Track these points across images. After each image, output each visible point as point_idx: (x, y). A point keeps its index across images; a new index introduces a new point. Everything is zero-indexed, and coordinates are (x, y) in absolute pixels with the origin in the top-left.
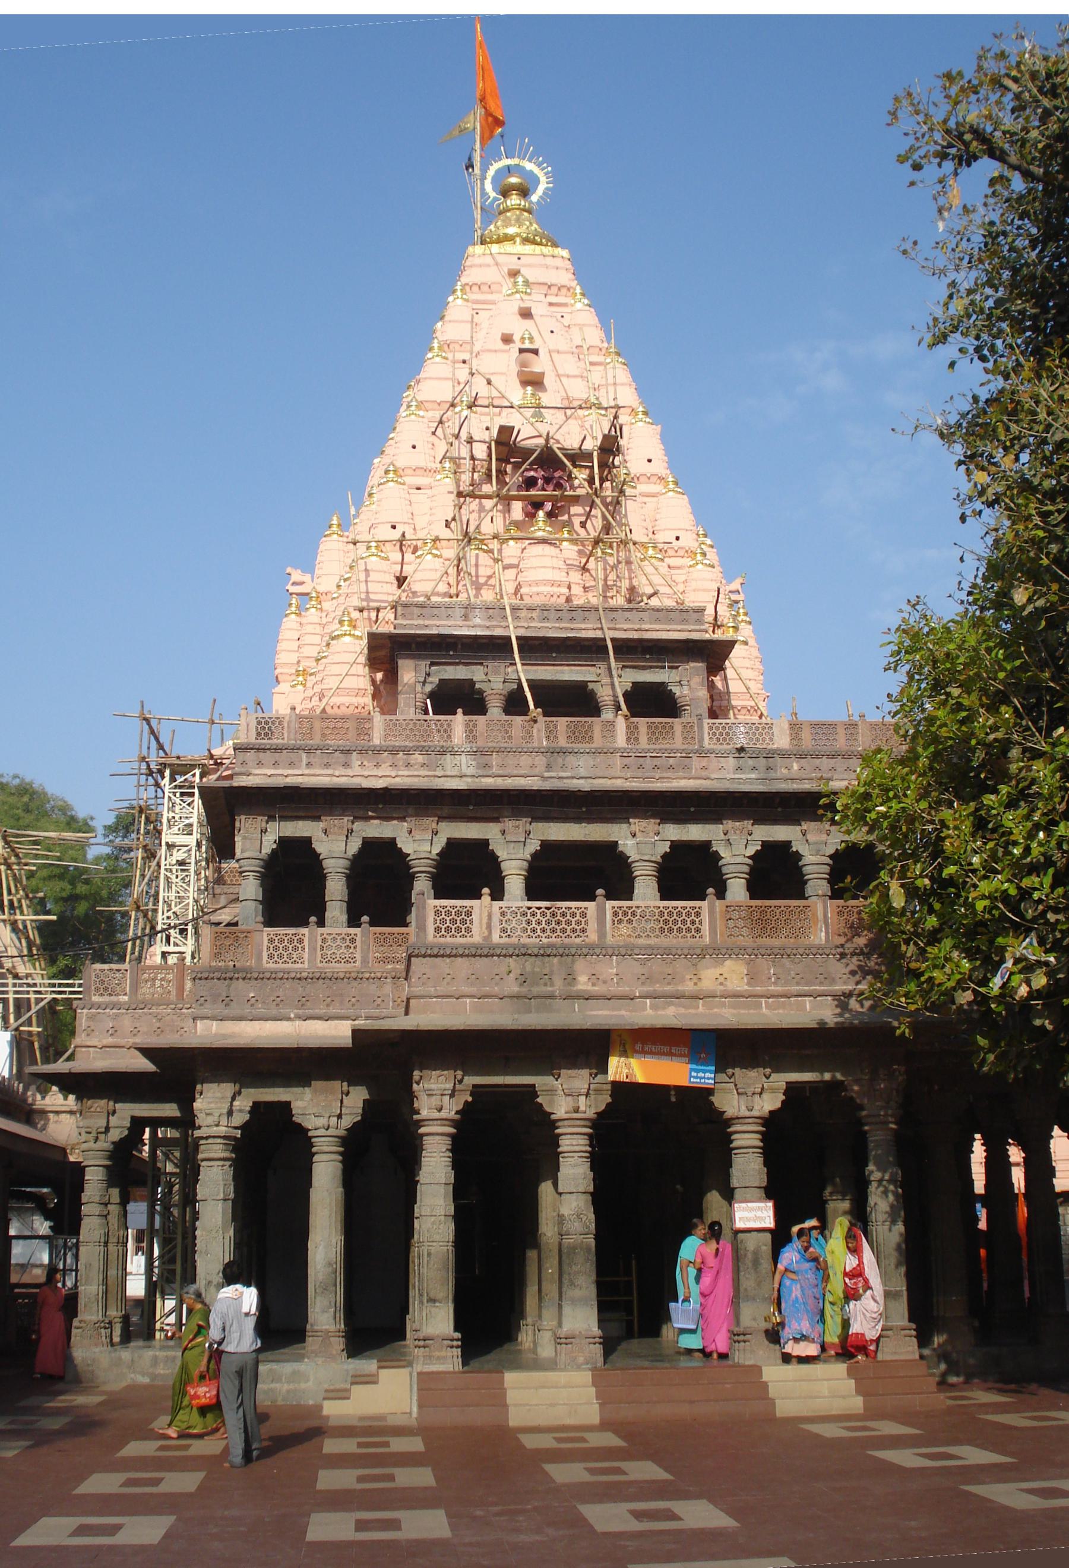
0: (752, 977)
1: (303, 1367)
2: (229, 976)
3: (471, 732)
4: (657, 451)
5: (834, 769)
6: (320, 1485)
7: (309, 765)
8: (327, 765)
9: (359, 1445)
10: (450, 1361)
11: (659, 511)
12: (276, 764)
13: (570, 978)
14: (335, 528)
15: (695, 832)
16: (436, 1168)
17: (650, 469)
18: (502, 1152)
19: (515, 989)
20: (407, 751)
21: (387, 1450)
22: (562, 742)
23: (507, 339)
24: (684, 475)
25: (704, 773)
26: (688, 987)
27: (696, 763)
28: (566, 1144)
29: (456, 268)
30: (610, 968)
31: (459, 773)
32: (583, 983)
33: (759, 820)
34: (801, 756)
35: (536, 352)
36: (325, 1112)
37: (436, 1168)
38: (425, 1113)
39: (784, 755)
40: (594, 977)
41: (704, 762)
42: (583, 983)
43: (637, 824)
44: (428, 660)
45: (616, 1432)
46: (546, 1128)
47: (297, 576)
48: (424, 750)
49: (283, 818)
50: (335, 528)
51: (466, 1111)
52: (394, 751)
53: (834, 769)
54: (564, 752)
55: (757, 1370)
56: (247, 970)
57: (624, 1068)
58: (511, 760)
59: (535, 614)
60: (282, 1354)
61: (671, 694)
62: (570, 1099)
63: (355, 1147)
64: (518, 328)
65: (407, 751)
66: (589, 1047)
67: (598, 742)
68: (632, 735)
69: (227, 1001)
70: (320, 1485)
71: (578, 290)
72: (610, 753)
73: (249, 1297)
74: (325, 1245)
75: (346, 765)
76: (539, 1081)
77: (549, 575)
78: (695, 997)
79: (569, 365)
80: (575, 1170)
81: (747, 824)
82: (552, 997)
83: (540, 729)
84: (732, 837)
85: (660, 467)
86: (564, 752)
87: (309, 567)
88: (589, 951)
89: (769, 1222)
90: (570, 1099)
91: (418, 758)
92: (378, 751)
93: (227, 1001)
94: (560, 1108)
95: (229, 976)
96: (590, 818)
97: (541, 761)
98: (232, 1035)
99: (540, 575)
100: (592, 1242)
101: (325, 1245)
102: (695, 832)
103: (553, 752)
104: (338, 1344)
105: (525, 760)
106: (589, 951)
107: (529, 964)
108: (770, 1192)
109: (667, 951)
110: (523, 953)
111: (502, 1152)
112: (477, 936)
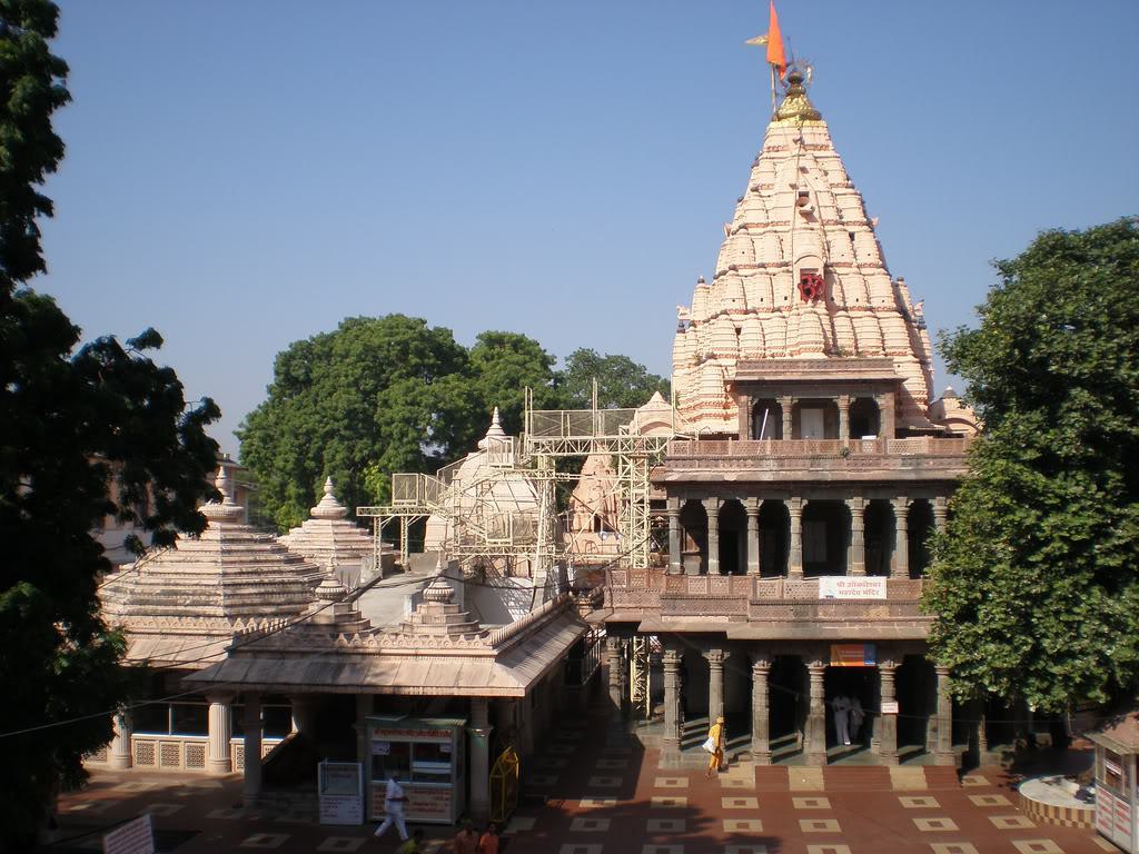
0: (891, 614)
2: (675, 598)
3: (774, 447)
5: (950, 464)
7: (699, 466)
8: (707, 466)
9: (736, 803)
10: (766, 763)
13: (816, 614)
20: (745, 459)
21: (743, 807)
22: (818, 452)
25: (886, 467)
26: (864, 617)
27: (883, 461)
28: (813, 679)
29: (764, 136)
40: (825, 614)
41: (887, 461)
42: (821, 616)
44: (766, 399)
48: (753, 458)
52: (739, 459)
53: (950, 464)
54: (818, 458)
55: (887, 769)
56: (682, 595)
58: (794, 462)
59: (806, 364)
60: (695, 752)
65: (745, 459)
69: (674, 608)
75: (716, 466)
77: (813, 338)
78: (866, 621)
82: (807, 621)
86: (818, 458)
87: (689, 305)
89: (896, 711)
93: (674, 608)
95: (675, 598)
97: (808, 462)
100: (823, 716)
103: (813, 458)
107: (798, 607)
108: (896, 698)
112: (777, 596)
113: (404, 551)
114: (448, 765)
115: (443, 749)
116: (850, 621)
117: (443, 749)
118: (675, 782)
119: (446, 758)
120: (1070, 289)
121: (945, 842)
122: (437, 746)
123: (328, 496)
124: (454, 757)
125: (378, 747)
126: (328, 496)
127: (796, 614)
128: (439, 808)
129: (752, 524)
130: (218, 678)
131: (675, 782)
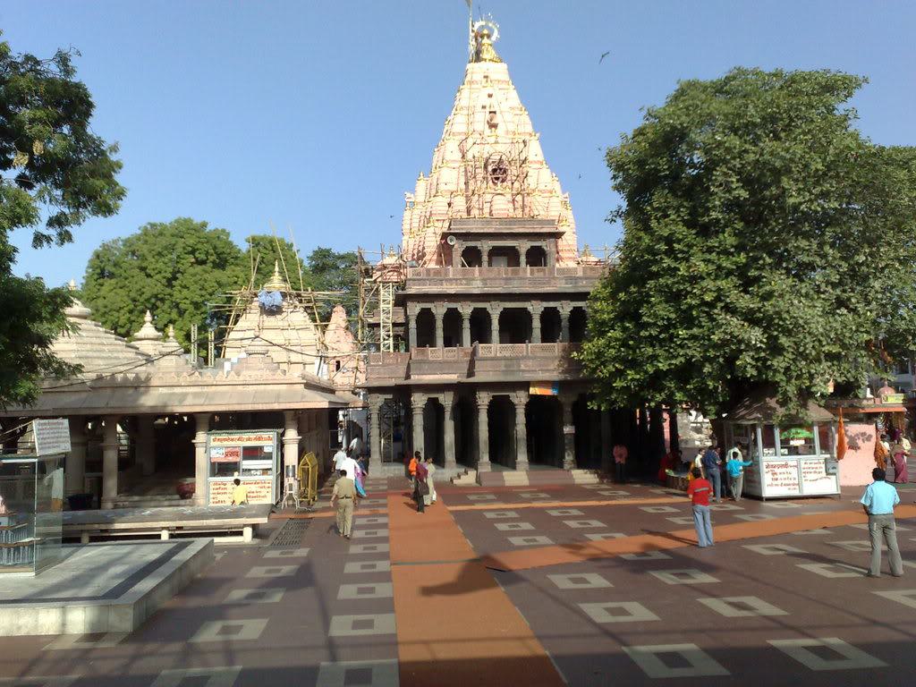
1: (444, 471)
4: (540, 152)
6: (346, 571)
11: (541, 177)
12: (419, 285)
14: (422, 177)
15: (552, 304)
16: (483, 418)
17: (536, 159)
18: (501, 411)
19: (504, 369)
22: (510, 276)
23: (484, 107)
24: (551, 160)
28: (518, 411)
30: (530, 363)
31: (476, 287)
32: (523, 367)
33: (572, 301)
34: (586, 279)
35: (495, 112)
36: (447, 400)
37: (483, 418)
38: (479, 403)
39: (580, 278)
40: (526, 366)
42: (523, 367)
43: (533, 302)
44: (469, 246)
45: (517, 512)
46: (512, 407)
47: (408, 195)
49: (423, 302)
50: (422, 177)
51: (491, 402)
52: (457, 280)
54: (510, 279)
57: (533, 391)
58: (493, 282)
61: (543, 250)
62: (520, 399)
63: (455, 408)
64: (487, 102)
66: (525, 385)
67: (521, 274)
68: (532, 273)
70: (346, 571)
71: (511, 82)
72: (526, 279)
73: (831, 390)
74: (449, 437)
75: (442, 285)
76: (511, 394)
79: (508, 117)
80: (521, 419)
81: (569, 302)
83: (501, 268)
84: (564, 306)
85: (541, 158)
86: (510, 279)
87: (413, 191)
88: (524, 358)
90: (520, 399)
91: (464, 282)
92: (451, 280)
94: (516, 401)
96: (519, 300)
97: (503, 282)
98: (421, 380)
99: (499, 206)
101: (449, 437)
102: (552, 304)
103: (507, 279)
104: (454, 464)
105: (498, 282)
106: (524, 358)
109: (546, 358)
110: (505, 358)
111: (501, 411)
112: (493, 355)
113: (725, 170)
114: (270, 462)
115: (266, 450)
116: (542, 370)
117: (266, 450)
118: (372, 590)
119: (269, 456)
120: (734, 171)
121: (635, 623)
122: (261, 448)
123: (148, 324)
124: (274, 456)
125: (216, 451)
126: (148, 324)
127: (506, 366)
128: (262, 494)
129: (466, 325)
130: (85, 405)
131: (372, 590)
